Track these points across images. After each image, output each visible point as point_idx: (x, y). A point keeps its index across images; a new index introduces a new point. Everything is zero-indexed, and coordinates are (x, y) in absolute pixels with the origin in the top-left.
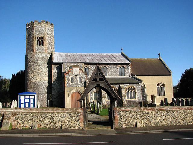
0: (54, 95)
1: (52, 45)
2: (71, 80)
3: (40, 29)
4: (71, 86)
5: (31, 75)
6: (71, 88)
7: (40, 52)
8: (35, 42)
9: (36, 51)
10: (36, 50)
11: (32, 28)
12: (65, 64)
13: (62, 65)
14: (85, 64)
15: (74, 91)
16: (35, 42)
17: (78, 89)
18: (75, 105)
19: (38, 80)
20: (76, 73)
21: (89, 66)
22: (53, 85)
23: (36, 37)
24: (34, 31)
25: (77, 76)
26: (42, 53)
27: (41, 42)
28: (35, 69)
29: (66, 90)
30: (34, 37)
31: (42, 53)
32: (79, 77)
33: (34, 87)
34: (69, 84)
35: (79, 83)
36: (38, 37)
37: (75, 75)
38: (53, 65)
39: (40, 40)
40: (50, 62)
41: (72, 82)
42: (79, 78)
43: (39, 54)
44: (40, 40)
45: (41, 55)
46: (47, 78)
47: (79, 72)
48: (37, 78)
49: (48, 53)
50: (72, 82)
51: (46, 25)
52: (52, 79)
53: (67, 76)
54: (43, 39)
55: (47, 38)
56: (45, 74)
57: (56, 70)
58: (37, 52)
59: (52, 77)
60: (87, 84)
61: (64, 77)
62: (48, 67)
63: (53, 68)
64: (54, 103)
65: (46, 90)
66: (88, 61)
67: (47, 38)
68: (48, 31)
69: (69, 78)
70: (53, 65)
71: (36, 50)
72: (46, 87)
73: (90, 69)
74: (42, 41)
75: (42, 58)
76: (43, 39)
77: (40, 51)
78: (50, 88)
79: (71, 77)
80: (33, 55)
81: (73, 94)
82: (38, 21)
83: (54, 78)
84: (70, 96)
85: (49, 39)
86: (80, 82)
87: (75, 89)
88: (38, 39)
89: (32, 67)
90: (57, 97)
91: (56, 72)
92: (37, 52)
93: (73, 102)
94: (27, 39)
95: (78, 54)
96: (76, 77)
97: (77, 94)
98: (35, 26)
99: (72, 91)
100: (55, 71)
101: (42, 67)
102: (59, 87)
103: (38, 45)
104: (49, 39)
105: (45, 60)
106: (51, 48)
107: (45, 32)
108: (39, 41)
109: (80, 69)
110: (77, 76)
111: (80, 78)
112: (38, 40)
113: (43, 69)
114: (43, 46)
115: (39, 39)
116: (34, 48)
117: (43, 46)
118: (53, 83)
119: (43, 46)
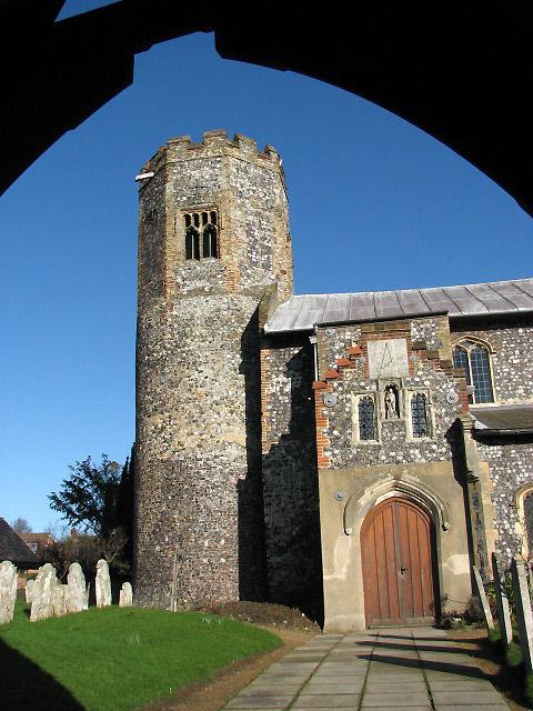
0: (277, 531)
1: (269, 251)
2: (356, 419)
3: (196, 174)
4: (356, 459)
5: (151, 420)
6: (357, 470)
7: (199, 292)
8: (176, 242)
9: (178, 285)
10: (179, 280)
11: (159, 179)
12: (332, 331)
13: (313, 340)
14: (459, 325)
15: (382, 491)
16: (176, 242)
17: (409, 480)
18: (392, 589)
19: (189, 442)
20: (386, 372)
21: (486, 337)
22: (269, 466)
23: (180, 215)
24: (169, 188)
25: (396, 393)
26: (207, 295)
27: (205, 240)
28: (173, 384)
29: (327, 488)
30: (170, 220)
31: (210, 293)
32: (410, 396)
33: (168, 487)
34: (347, 445)
35: (411, 437)
36: (187, 217)
37: (382, 386)
38: (265, 352)
39: (200, 230)
40: (255, 340)
41: (367, 430)
42: (409, 406)
43: (194, 300)
44: (200, 230)
45: (201, 308)
46: (240, 434)
47: (410, 362)
48: (182, 436)
49: (246, 293)
50: (364, 436)
51: (235, 152)
52: (264, 433)
53: (333, 398)
54: (214, 221)
55: (236, 214)
56: (224, 410)
57: (282, 378)
58: (185, 291)
59: (264, 420)
60: (296, 352)
61: (313, 400)
62: (243, 369)
63: (265, 367)
64: (276, 578)
65: (231, 499)
66: (477, 309)
67: (235, 220)
68: (243, 183)
69: (344, 406)
70: (265, 352)
71: (179, 280)
72: (233, 480)
73: (493, 360)
74: (212, 232)
75: (209, 322)
76: (214, 221)
77: (199, 284)
78: (252, 492)
79: (356, 400)
80: (162, 312)
81: (375, 512)
82: (188, 138)
83: (274, 427)
84: (356, 527)
85: (251, 218)
86: (419, 432)
87: (390, 481)
88: (188, 223)
89: (156, 379)
90: (293, 541)
91: (288, 389)
92: (185, 291)
93: (381, 573)
94: (142, 237)
95: (425, 291)
96: (392, 397)
97: (402, 510)
98: (173, 164)
99: (367, 495)
100: (277, 384)
101: (208, 371)
102: (304, 480)
103: (188, 257)
104: (251, 218)
105: (224, 330)
106: (267, 267)
107: (225, 186)
108: (196, 234)
109: (417, 347)
110: (396, 393)
111: (420, 404)
112: (191, 234)
113: (220, 378)
114: (216, 254)
115: (197, 224)
116: (169, 274)
117: (213, 260)
118: (267, 457)
119: (216, 254)
